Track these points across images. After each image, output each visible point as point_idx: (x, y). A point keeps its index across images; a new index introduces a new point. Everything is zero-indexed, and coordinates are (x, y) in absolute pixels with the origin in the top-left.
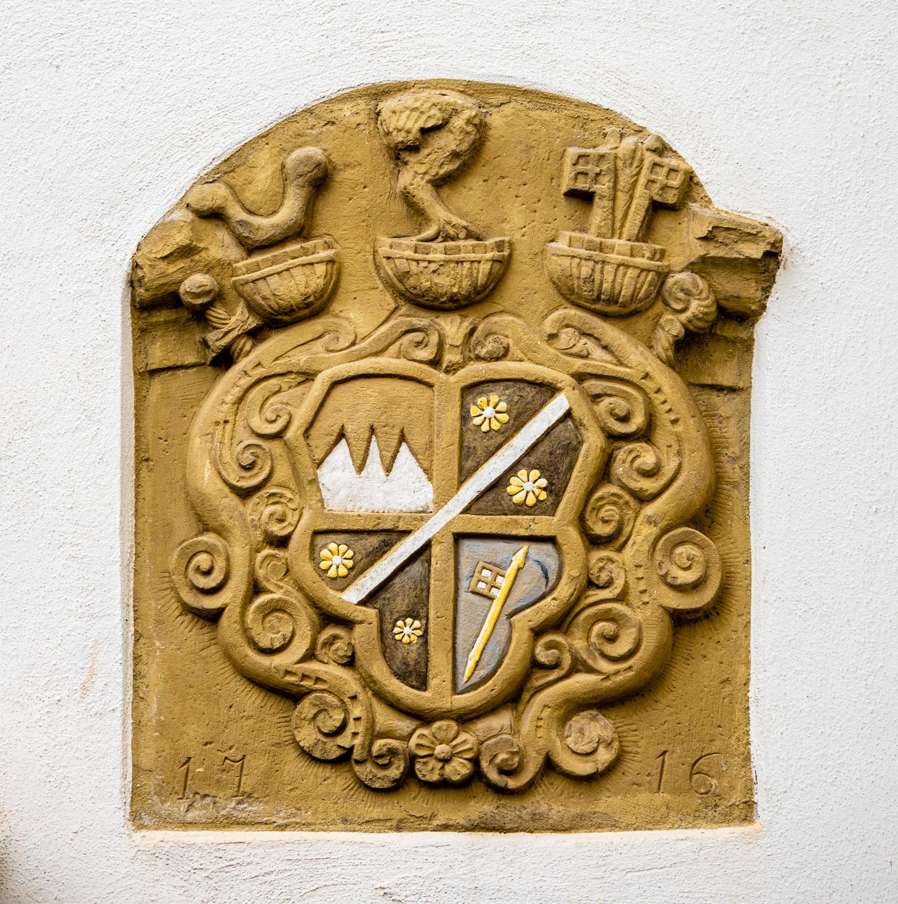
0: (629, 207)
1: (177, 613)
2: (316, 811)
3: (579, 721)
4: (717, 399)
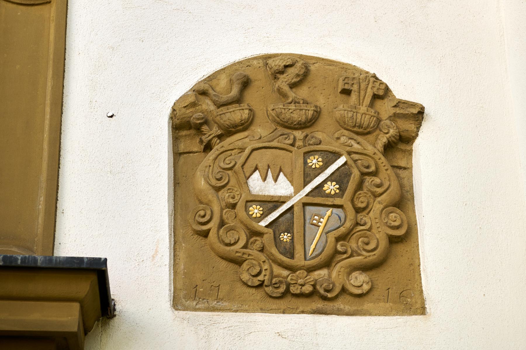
0: (365, 96)
1: (191, 234)
2: (249, 306)
3: (355, 274)
4: (400, 172)
